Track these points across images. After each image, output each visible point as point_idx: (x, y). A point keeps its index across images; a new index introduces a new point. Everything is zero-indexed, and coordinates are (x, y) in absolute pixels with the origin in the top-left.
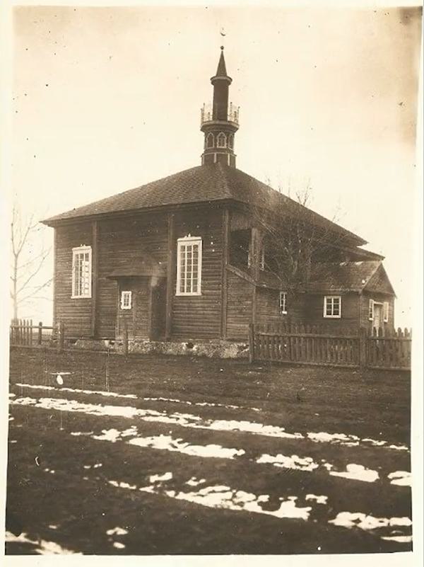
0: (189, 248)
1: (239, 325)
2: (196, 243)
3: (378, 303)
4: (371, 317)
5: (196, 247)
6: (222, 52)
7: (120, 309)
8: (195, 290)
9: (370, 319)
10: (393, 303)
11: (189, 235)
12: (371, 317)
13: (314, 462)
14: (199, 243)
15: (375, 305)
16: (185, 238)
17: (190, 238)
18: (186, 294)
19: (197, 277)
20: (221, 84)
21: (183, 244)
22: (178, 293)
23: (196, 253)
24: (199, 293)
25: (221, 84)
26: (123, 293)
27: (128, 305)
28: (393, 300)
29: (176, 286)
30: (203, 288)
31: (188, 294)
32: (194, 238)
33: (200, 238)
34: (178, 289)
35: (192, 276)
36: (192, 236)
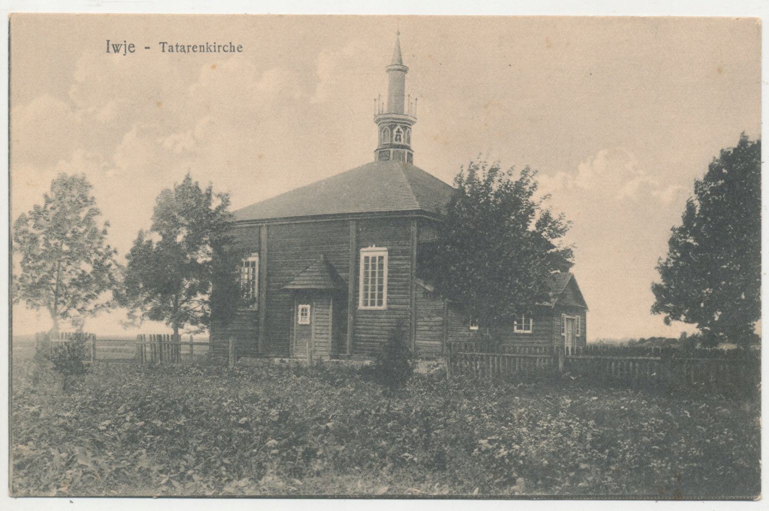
0: (374, 259)
1: (432, 343)
2: (381, 254)
3: (569, 317)
4: (563, 332)
5: (381, 258)
6: (398, 41)
7: (297, 323)
8: (380, 303)
9: (563, 334)
10: (585, 316)
11: (374, 246)
12: (563, 332)
13: (34, 283)
14: (385, 255)
15: (567, 318)
16: (369, 248)
17: (374, 248)
18: (369, 307)
19: (382, 268)
20: (400, 70)
21: (366, 254)
22: (361, 307)
23: (381, 266)
24: (384, 307)
25: (400, 70)
26: (301, 307)
27: (303, 310)
28: (585, 313)
29: (358, 296)
30: (388, 304)
31: (373, 308)
32: (378, 249)
33: (385, 249)
34: (361, 302)
35: (376, 295)
36: (376, 246)
